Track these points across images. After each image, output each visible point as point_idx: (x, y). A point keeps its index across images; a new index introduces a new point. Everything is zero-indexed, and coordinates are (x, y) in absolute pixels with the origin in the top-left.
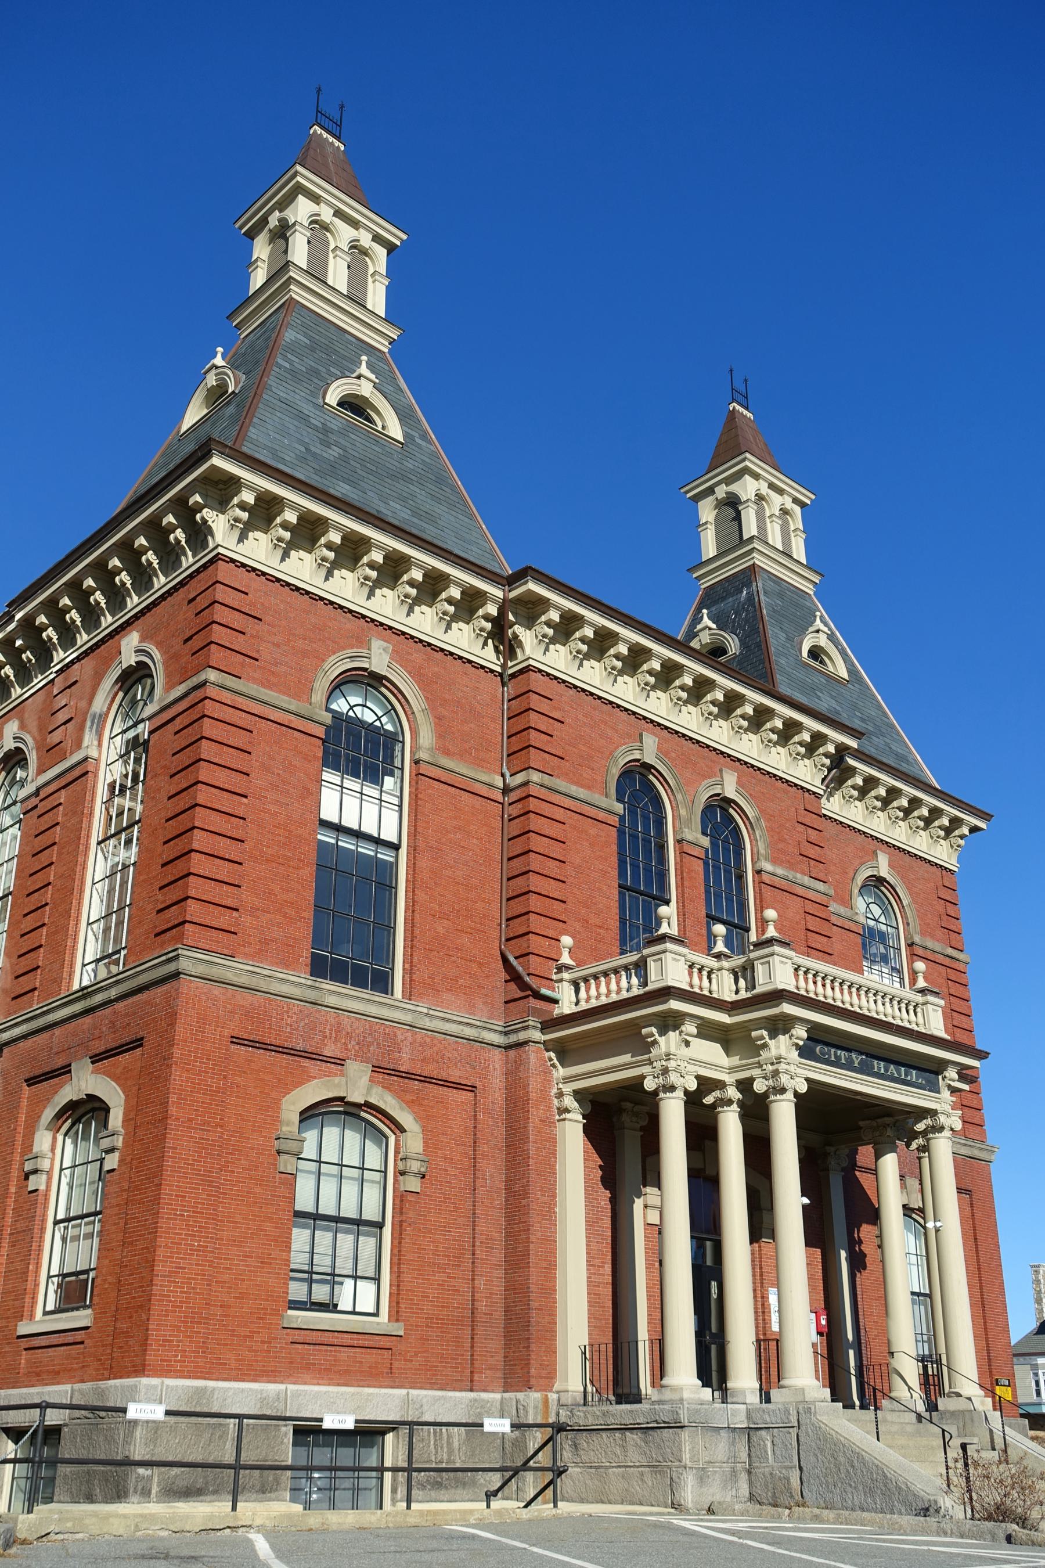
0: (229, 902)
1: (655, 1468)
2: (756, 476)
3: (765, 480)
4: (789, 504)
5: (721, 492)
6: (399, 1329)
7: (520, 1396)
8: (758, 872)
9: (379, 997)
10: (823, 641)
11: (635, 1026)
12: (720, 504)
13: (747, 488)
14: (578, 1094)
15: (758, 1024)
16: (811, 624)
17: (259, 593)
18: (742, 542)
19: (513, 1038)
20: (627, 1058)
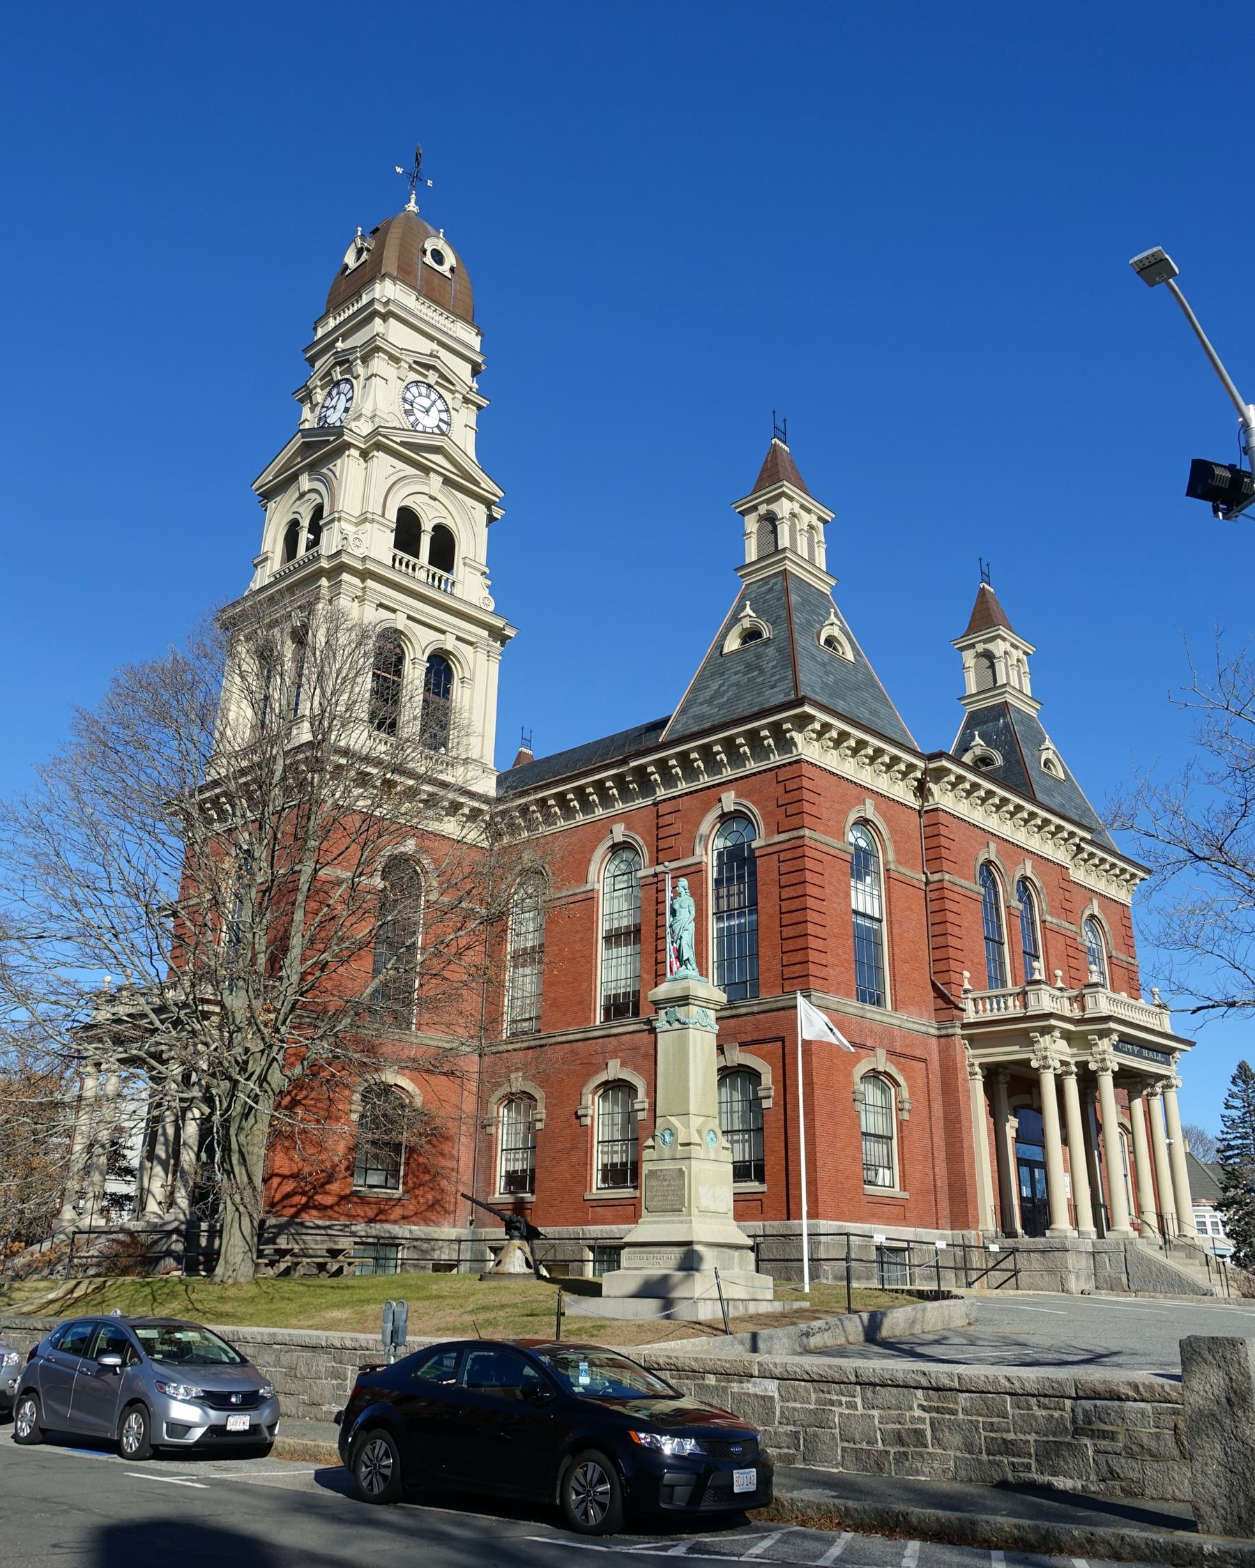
0: (824, 962)
1: (1051, 1272)
2: (791, 499)
3: (798, 502)
4: (815, 522)
5: (763, 509)
6: (906, 1195)
7: (965, 1232)
8: (1044, 922)
9: (875, 1008)
10: (836, 632)
11: (1026, 1031)
12: (762, 518)
13: (784, 508)
14: (981, 1065)
15: (1092, 1032)
16: (827, 619)
17: (822, 782)
18: (777, 551)
19: (944, 1032)
20: (1017, 1048)
